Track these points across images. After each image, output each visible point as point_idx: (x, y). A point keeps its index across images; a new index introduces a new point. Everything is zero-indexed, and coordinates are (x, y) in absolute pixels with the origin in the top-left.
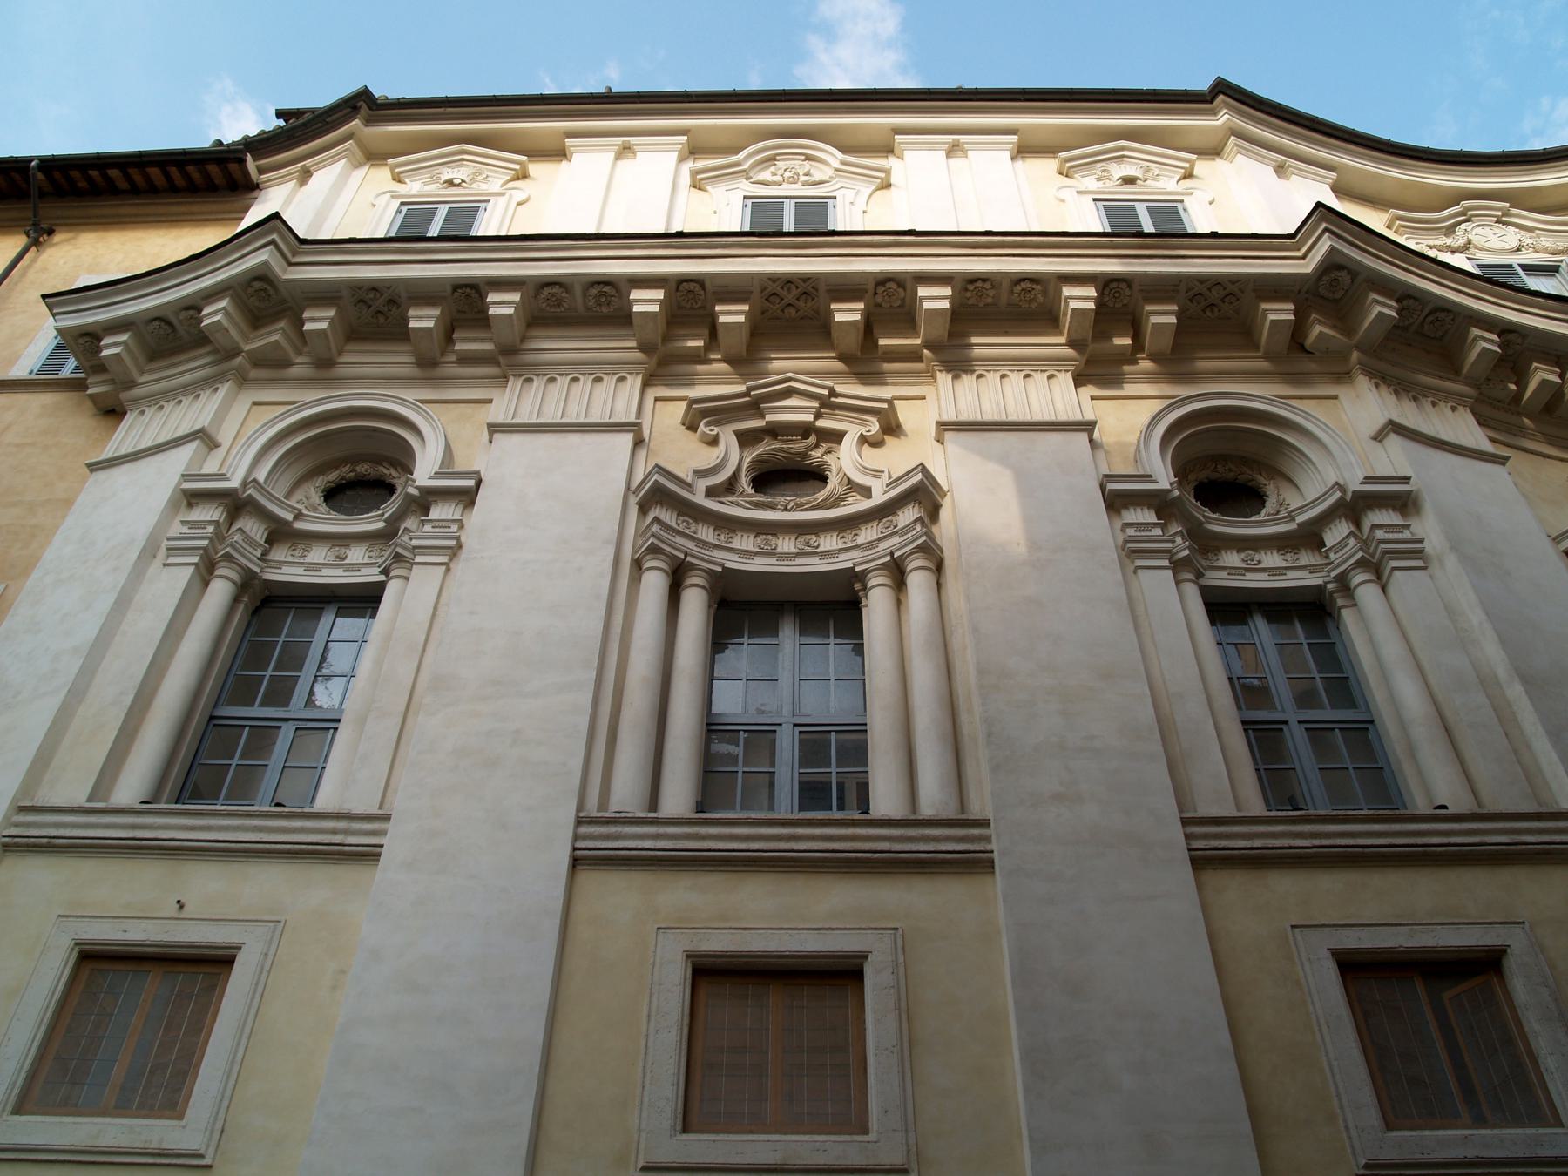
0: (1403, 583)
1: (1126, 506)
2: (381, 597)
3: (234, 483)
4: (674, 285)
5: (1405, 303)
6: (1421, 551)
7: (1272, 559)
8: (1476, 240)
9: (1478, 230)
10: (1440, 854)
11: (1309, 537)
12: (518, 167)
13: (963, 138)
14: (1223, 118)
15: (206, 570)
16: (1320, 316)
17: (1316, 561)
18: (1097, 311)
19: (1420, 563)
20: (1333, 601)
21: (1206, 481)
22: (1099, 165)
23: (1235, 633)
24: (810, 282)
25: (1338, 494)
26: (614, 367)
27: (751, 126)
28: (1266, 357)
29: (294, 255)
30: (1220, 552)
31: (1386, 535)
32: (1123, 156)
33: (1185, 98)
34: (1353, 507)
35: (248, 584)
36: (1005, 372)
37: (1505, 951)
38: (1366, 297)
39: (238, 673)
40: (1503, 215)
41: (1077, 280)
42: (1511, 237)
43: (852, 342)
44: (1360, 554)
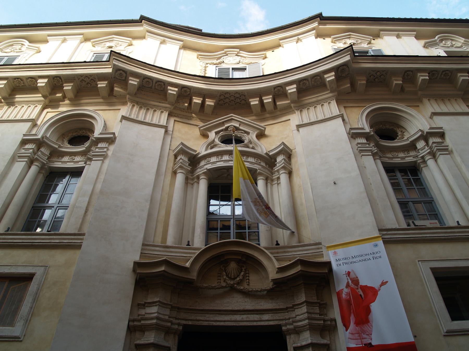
0: (441, 159)
1: (357, 137)
2: (83, 172)
3: (39, 137)
4: (142, 78)
6: (447, 149)
10: (38, 245)
11: (412, 146)
12: (129, 42)
13: (67, 37)
14: (145, 27)
15: (31, 162)
16: (117, 85)
17: (414, 154)
18: (430, 79)
19: (447, 153)
20: (419, 165)
22: (103, 43)
24: (93, 76)
25: (420, 133)
26: (325, 100)
28: (103, 98)
31: (25, 151)
32: (113, 40)
33: (28, 26)
34: (425, 137)
35: (42, 168)
36: (23, 105)
39: (41, 193)
40: (238, 53)
41: (44, 77)
43: (105, 93)
44: (429, 150)
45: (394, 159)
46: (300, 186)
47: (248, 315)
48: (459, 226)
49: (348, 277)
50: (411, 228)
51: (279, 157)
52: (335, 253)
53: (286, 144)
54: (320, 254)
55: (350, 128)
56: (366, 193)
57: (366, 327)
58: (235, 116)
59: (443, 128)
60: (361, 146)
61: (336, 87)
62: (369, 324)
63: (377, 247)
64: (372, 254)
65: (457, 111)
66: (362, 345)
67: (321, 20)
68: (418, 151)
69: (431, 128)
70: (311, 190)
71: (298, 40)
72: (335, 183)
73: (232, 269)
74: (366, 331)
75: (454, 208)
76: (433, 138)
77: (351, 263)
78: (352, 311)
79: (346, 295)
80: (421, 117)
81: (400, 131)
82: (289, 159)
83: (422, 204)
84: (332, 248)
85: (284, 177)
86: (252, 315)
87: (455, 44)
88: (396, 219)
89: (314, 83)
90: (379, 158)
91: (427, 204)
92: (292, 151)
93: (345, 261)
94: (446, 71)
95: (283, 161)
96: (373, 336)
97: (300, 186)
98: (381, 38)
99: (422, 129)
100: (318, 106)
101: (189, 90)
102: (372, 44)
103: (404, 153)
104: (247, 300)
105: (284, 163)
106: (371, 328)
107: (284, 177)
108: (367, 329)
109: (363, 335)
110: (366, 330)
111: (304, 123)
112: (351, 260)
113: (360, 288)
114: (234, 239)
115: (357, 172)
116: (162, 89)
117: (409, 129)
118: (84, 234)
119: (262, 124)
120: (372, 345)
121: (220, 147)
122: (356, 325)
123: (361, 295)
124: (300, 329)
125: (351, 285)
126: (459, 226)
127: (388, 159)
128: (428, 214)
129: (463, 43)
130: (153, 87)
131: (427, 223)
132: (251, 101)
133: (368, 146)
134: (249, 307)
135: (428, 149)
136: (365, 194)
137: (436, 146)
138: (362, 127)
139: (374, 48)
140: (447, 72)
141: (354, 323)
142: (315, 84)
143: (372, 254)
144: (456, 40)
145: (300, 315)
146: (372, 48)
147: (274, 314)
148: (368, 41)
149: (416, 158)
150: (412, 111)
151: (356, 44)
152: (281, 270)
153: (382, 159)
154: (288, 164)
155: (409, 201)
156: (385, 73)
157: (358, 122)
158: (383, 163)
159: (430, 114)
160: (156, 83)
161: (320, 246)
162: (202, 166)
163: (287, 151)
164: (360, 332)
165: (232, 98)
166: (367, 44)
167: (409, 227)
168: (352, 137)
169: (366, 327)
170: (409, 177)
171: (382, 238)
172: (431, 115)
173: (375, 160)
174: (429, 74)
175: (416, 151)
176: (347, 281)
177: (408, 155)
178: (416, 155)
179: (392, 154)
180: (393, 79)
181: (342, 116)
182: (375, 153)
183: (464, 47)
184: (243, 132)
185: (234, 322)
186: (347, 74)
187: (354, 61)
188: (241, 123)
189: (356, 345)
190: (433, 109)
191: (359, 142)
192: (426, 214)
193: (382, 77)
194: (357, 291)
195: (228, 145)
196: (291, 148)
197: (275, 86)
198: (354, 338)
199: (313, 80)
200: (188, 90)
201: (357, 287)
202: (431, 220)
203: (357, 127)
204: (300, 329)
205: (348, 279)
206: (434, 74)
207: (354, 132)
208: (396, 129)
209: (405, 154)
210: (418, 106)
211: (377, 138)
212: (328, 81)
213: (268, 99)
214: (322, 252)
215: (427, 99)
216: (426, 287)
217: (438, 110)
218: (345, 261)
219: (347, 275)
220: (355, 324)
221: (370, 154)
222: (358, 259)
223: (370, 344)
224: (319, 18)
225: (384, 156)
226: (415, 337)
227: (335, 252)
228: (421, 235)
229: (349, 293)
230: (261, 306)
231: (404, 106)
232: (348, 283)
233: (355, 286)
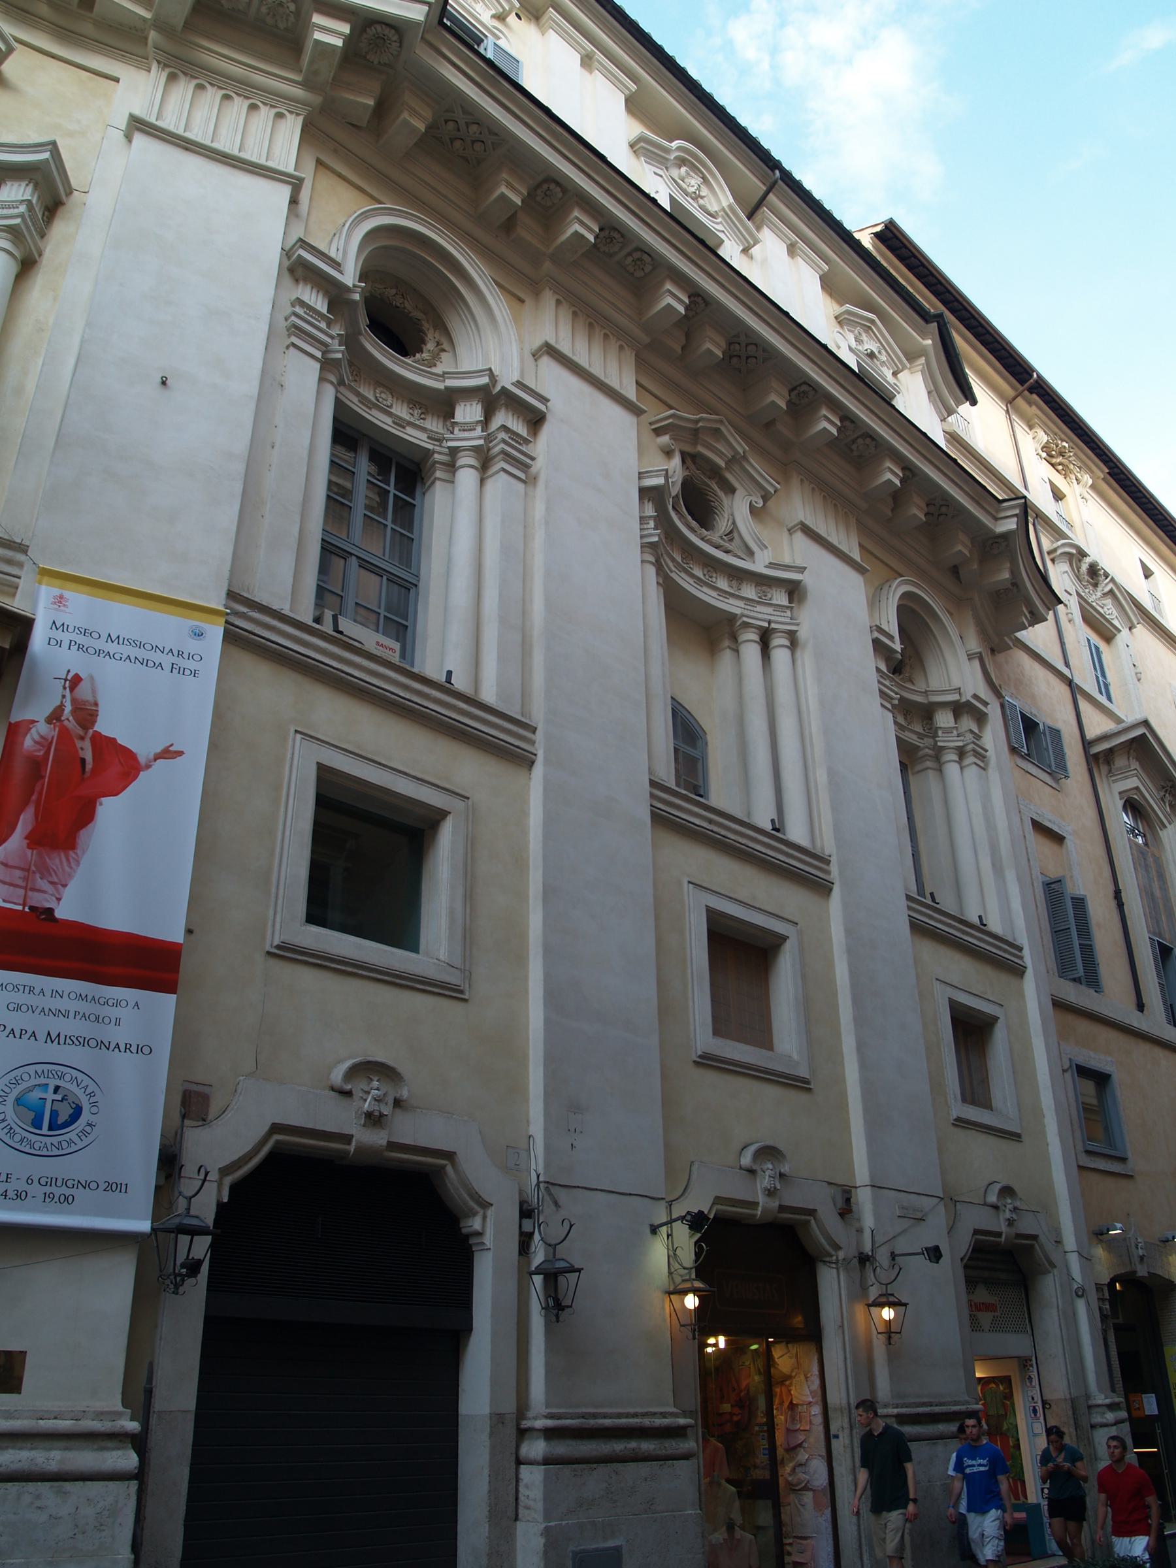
0: (500, 484)
1: (306, 280)
6: (528, 466)
18: (595, 245)
19: (523, 476)
21: (379, 297)
23: (345, 455)
25: (485, 380)
26: (273, 98)
27: (857, 282)
29: (998, 511)
34: (959, 709)
37: (997, 1020)
38: (571, 211)
44: (481, 442)
45: (374, 412)
46: (43, 330)
48: (448, 685)
49: (68, 689)
50: (320, 630)
51: (12, 185)
52: (60, 600)
53: (63, 157)
54: (6, 580)
55: (300, 240)
56: (244, 466)
57: (57, 861)
59: (549, 404)
60: (303, 314)
61: (330, 80)
62: (71, 853)
63: (201, 640)
64: (176, 654)
65: (607, 381)
66: (24, 908)
68: (451, 429)
69: (520, 384)
70: (72, 361)
72: (164, 383)
74: (54, 870)
75: (457, 633)
76: (510, 414)
77: (98, 652)
78: (34, 797)
79: (36, 742)
80: (513, 337)
81: (435, 338)
82: (46, 213)
83: (382, 581)
84: (57, 582)
87: (704, 197)
88: (293, 586)
89: (268, 14)
90: (335, 381)
91: (396, 587)
92: (71, 193)
93: (80, 639)
94: (646, 253)
95: (23, 208)
96: (68, 893)
97: (43, 330)
98: (540, 28)
99: (496, 373)
100: (237, 100)
102: (507, 26)
103: (411, 411)
105: (22, 216)
106: (71, 868)
108: (59, 866)
109: (39, 880)
110: (55, 868)
111: (160, 124)
112: (100, 644)
113: (91, 739)
115: (253, 388)
117: (462, 350)
120: (53, 915)
122: (28, 844)
123: (83, 761)
125: (68, 719)
126: (446, 686)
127: (360, 401)
128: (385, 616)
129: (723, 210)
131: (369, 638)
133: (325, 328)
135: (480, 438)
136: (240, 467)
137: (504, 441)
138: (339, 259)
139: (502, 43)
140: (645, 257)
141: (24, 836)
142: (269, 20)
143: (176, 653)
144: (716, 192)
146: (499, 38)
148: (501, 10)
149: (436, 443)
150: (497, 304)
153: (342, 389)
154: (36, 230)
155: (351, 554)
156: (492, 143)
157: (335, 234)
158: (339, 405)
159: (537, 343)
161: (20, 557)
163: (54, 180)
164: (33, 868)
166: (493, 16)
167: (317, 626)
168: (291, 270)
169: (56, 861)
170: (389, 485)
171: (227, 622)
172: (540, 349)
173: (321, 379)
174: (601, 229)
175: (444, 425)
176: (58, 703)
177: (417, 422)
178: (440, 434)
179: (378, 395)
180: (504, 175)
181: (296, 184)
182: (332, 359)
183: (719, 220)
186: (385, 64)
187: (428, 37)
189: (4, 901)
190: (554, 335)
191: (306, 299)
192: (379, 614)
193: (478, 147)
194: (79, 744)
196: (74, 183)
198: (8, 880)
201: (81, 733)
202: (383, 634)
203: (322, 247)
205: (64, 697)
206: (612, 239)
207: (306, 260)
208: (428, 329)
209: (412, 415)
210: (522, 301)
211: (363, 321)
212: (317, 42)
214: (16, 580)
215: (557, 297)
216: (282, 809)
217: (565, 347)
218: (80, 639)
219: (68, 682)
220: (26, 838)
221: (319, 354)
222: (126, 650)
223: (50, 911)
225: (352, 384)
226: (189, 931)
227: (61, 597)
228: (340, 663)
229: (50, 740)
231: (488, 279)
232: (60, 709)
233: (79, 728)
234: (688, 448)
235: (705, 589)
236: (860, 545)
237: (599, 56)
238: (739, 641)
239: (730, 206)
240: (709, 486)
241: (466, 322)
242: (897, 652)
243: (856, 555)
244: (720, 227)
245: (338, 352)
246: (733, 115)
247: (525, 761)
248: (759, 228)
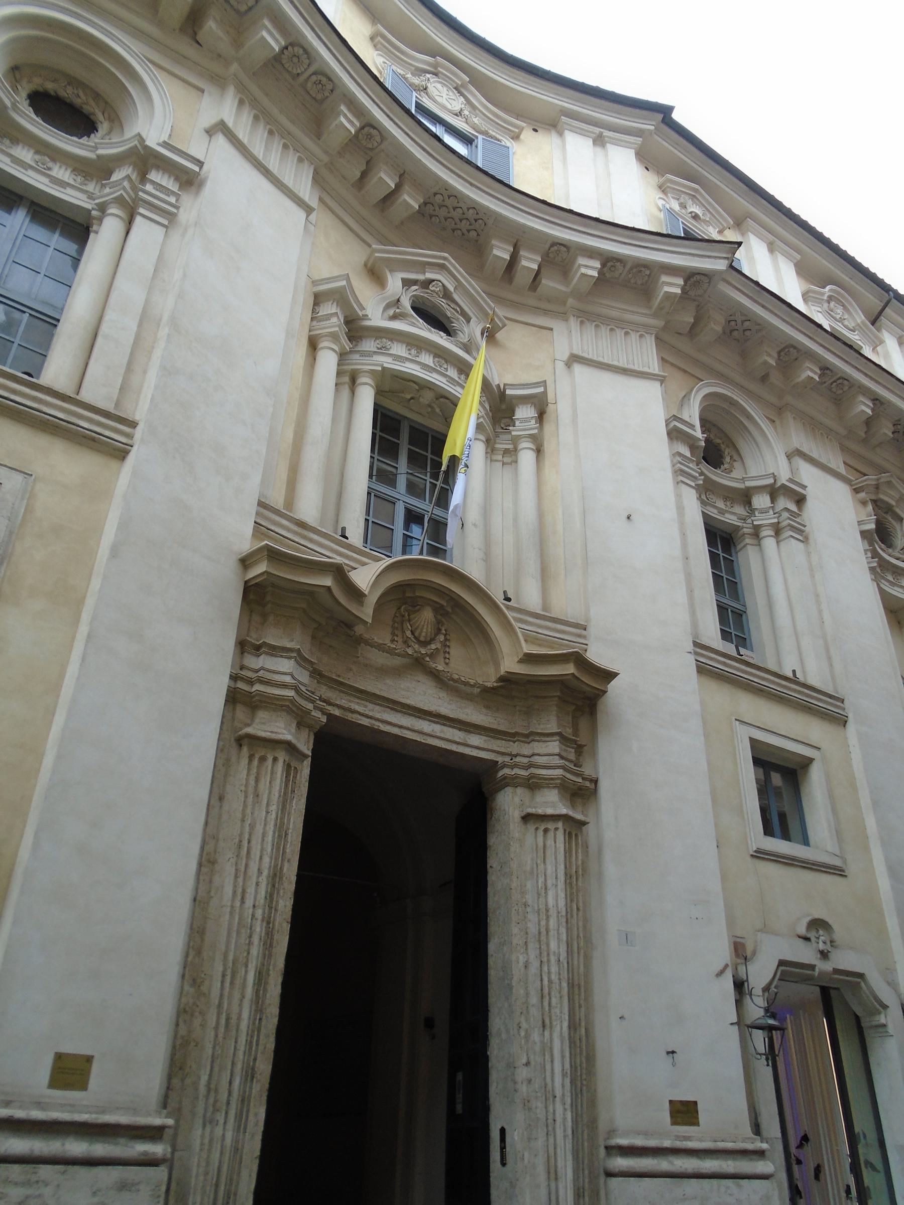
1: (677, 439)
5: (825, 371)
7: (62, 173)
8: (431, 88)
9: (439, 86)
11: (745, 497)
30: (18, 144)
34: (774, 491)
40: (462, 86)
42: (457, 104)
47: (443, 727)
58: (453, 264)
67: (663, 121)
71: (598, 136)
72: (628, 518)
73: (425, 622)
85: (527, 458)
86: (451, 729)
94: (845, 379)
101: (379, 141)
104: (443, 694)
107: (527, 458)
114: (421, 553)
116: (319, 97)
117: (749, 461)
118: (134, 422)
119: (501, 312)
121: (413, 325)
124: (541, 781)
129: (858, 325)
130: (302, 79)
132: (525, 257)
134: (446, 710)
145: (541, 755)
147: (489, 738)
151: (700, 218)
152: (529, 659)
155: (399, 500)
160: (314, 73)
162: (370, 351)
165: (456, 214)
177: (730, 510)
184: (458, 309)
185: (417, 734)
188: (459, 285)
195: (432, 329)
197: (556, 241)
199: (635, 270)
200: (378, 139)
204: (541, 781)
213: (529, 262)
224: (662, 116)
230: (467, 714)
234: (874, 497)
235: (896, 588)
236: (845, 463)
237: (778, 242)
238: (760, 537)
239: (863, 322)
240: (886, 519)
241: (749, 442)
242: (701, 440)
243: (842, 470)
244: (857, 337)
245: (700, 480)
246: (772, 194)
247: (121, 453)
248: (879, 330)
